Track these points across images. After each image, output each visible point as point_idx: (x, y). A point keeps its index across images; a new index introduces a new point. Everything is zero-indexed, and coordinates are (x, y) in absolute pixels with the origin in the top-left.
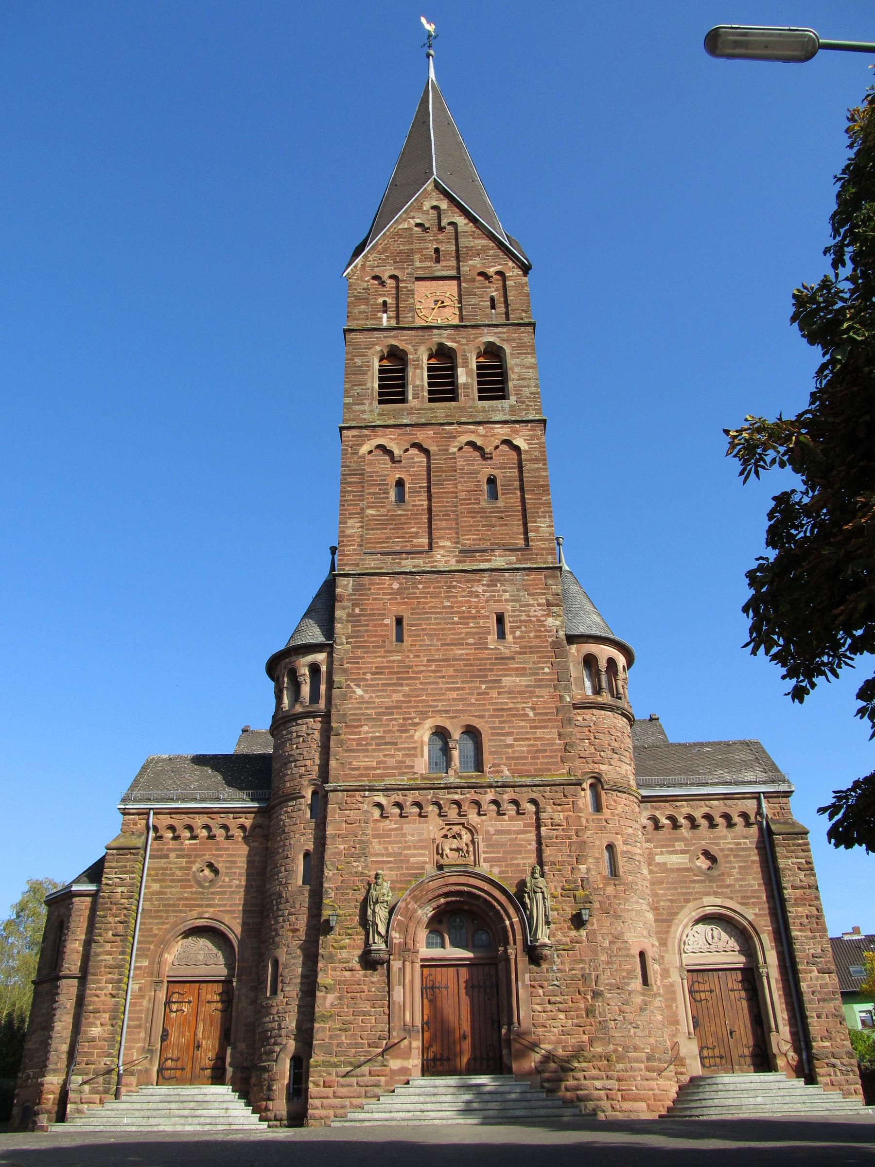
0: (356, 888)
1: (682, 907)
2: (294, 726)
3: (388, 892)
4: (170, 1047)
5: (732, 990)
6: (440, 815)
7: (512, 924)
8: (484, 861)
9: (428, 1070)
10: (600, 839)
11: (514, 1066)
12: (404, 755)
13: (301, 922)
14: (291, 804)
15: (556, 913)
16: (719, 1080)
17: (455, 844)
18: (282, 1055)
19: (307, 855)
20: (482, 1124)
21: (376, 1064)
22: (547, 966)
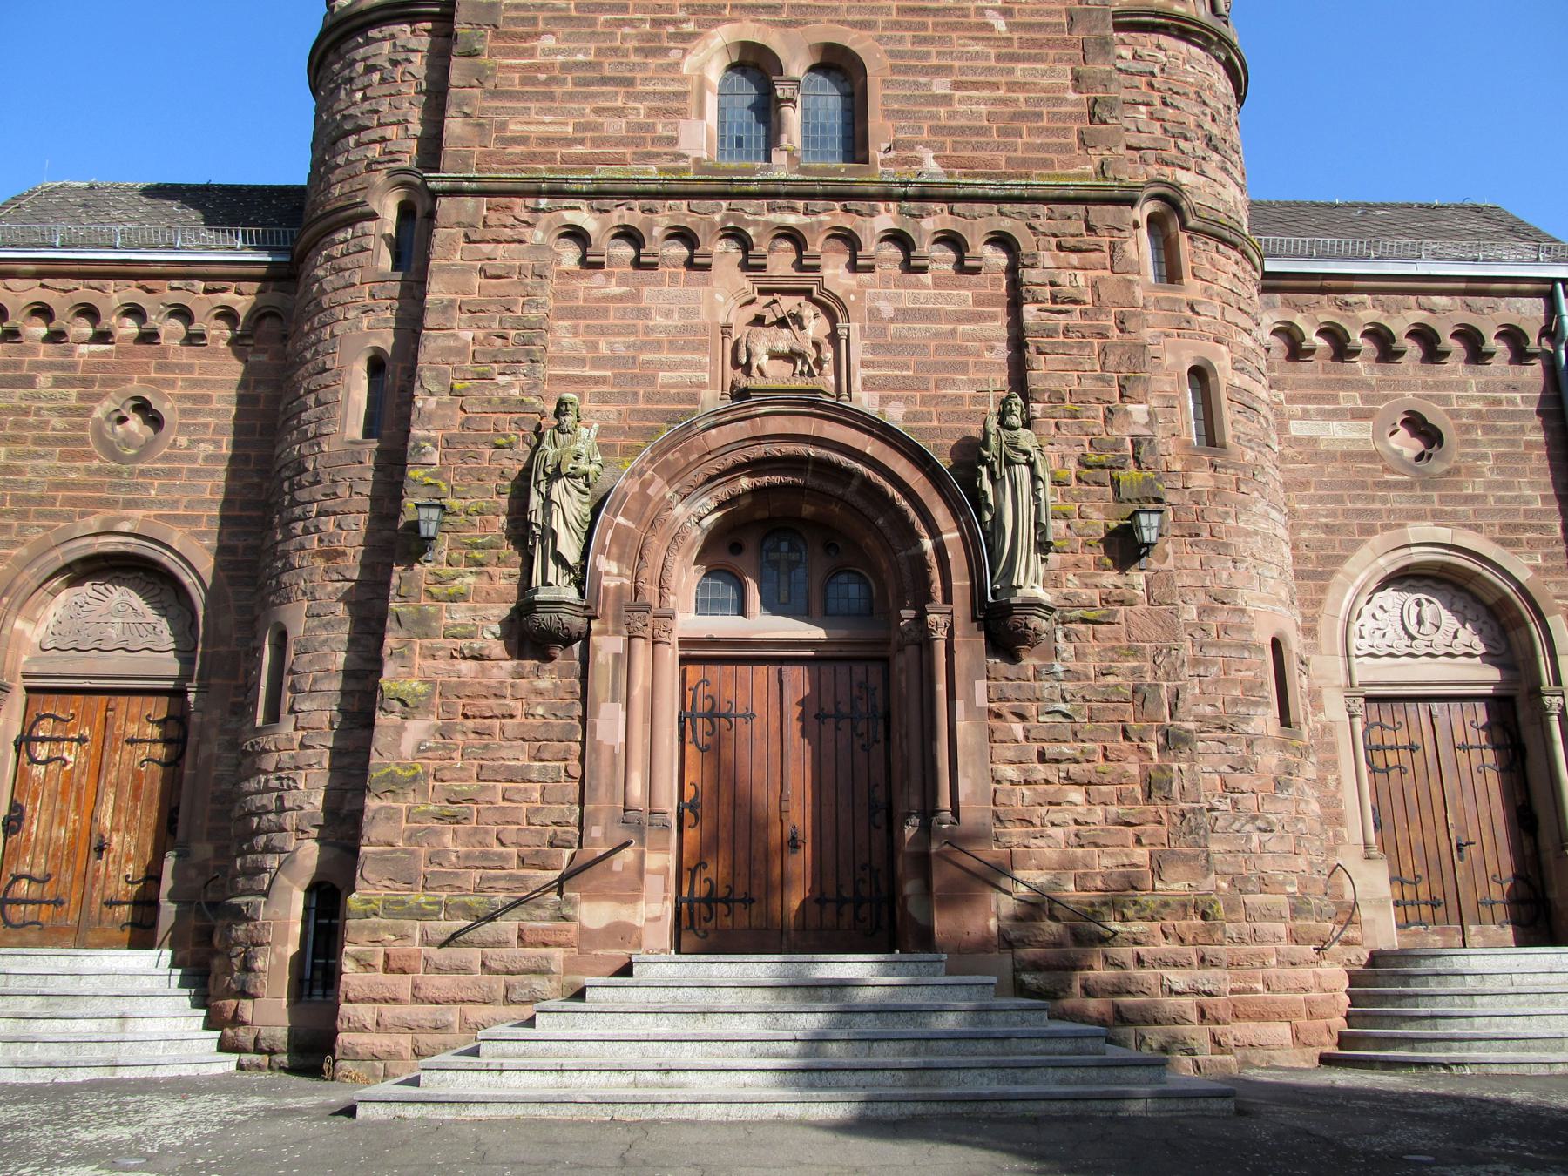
0: (502, 441)
1: (1355, 546)
2: (359, 46)
3: (591, 451)
4: (26, 849)
5: (1465, 747)
6: (745, 266)
7: (940, 549)
8: (865, 387)
9: (692, 926)
10: (1176, 352)
11: (938, 926)
12: (653, 112)
13: (352, 534)
14: (340, 236)
15: (1062, 524)
16: (1458, 963)
17: (784, 340)
18: (283, 879)
19: (377, 365)
20: (860, 1126)
21: (539, 912)
22: (1037, 662)
